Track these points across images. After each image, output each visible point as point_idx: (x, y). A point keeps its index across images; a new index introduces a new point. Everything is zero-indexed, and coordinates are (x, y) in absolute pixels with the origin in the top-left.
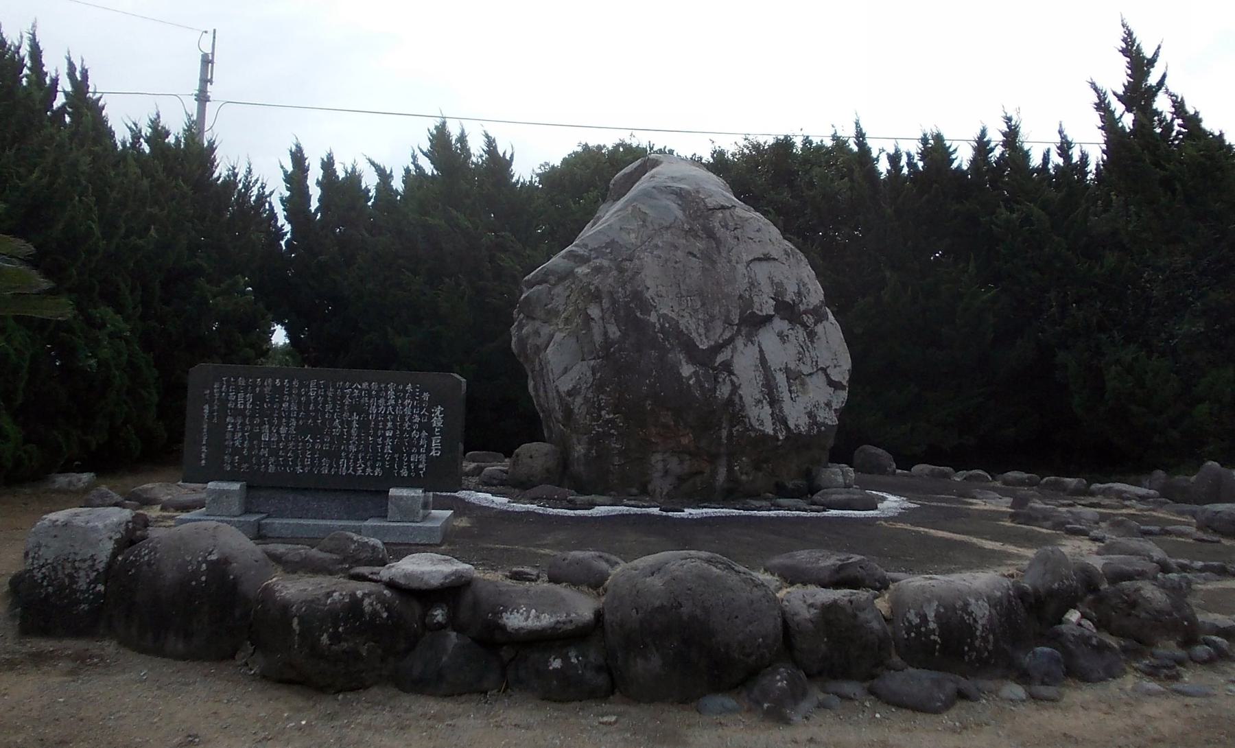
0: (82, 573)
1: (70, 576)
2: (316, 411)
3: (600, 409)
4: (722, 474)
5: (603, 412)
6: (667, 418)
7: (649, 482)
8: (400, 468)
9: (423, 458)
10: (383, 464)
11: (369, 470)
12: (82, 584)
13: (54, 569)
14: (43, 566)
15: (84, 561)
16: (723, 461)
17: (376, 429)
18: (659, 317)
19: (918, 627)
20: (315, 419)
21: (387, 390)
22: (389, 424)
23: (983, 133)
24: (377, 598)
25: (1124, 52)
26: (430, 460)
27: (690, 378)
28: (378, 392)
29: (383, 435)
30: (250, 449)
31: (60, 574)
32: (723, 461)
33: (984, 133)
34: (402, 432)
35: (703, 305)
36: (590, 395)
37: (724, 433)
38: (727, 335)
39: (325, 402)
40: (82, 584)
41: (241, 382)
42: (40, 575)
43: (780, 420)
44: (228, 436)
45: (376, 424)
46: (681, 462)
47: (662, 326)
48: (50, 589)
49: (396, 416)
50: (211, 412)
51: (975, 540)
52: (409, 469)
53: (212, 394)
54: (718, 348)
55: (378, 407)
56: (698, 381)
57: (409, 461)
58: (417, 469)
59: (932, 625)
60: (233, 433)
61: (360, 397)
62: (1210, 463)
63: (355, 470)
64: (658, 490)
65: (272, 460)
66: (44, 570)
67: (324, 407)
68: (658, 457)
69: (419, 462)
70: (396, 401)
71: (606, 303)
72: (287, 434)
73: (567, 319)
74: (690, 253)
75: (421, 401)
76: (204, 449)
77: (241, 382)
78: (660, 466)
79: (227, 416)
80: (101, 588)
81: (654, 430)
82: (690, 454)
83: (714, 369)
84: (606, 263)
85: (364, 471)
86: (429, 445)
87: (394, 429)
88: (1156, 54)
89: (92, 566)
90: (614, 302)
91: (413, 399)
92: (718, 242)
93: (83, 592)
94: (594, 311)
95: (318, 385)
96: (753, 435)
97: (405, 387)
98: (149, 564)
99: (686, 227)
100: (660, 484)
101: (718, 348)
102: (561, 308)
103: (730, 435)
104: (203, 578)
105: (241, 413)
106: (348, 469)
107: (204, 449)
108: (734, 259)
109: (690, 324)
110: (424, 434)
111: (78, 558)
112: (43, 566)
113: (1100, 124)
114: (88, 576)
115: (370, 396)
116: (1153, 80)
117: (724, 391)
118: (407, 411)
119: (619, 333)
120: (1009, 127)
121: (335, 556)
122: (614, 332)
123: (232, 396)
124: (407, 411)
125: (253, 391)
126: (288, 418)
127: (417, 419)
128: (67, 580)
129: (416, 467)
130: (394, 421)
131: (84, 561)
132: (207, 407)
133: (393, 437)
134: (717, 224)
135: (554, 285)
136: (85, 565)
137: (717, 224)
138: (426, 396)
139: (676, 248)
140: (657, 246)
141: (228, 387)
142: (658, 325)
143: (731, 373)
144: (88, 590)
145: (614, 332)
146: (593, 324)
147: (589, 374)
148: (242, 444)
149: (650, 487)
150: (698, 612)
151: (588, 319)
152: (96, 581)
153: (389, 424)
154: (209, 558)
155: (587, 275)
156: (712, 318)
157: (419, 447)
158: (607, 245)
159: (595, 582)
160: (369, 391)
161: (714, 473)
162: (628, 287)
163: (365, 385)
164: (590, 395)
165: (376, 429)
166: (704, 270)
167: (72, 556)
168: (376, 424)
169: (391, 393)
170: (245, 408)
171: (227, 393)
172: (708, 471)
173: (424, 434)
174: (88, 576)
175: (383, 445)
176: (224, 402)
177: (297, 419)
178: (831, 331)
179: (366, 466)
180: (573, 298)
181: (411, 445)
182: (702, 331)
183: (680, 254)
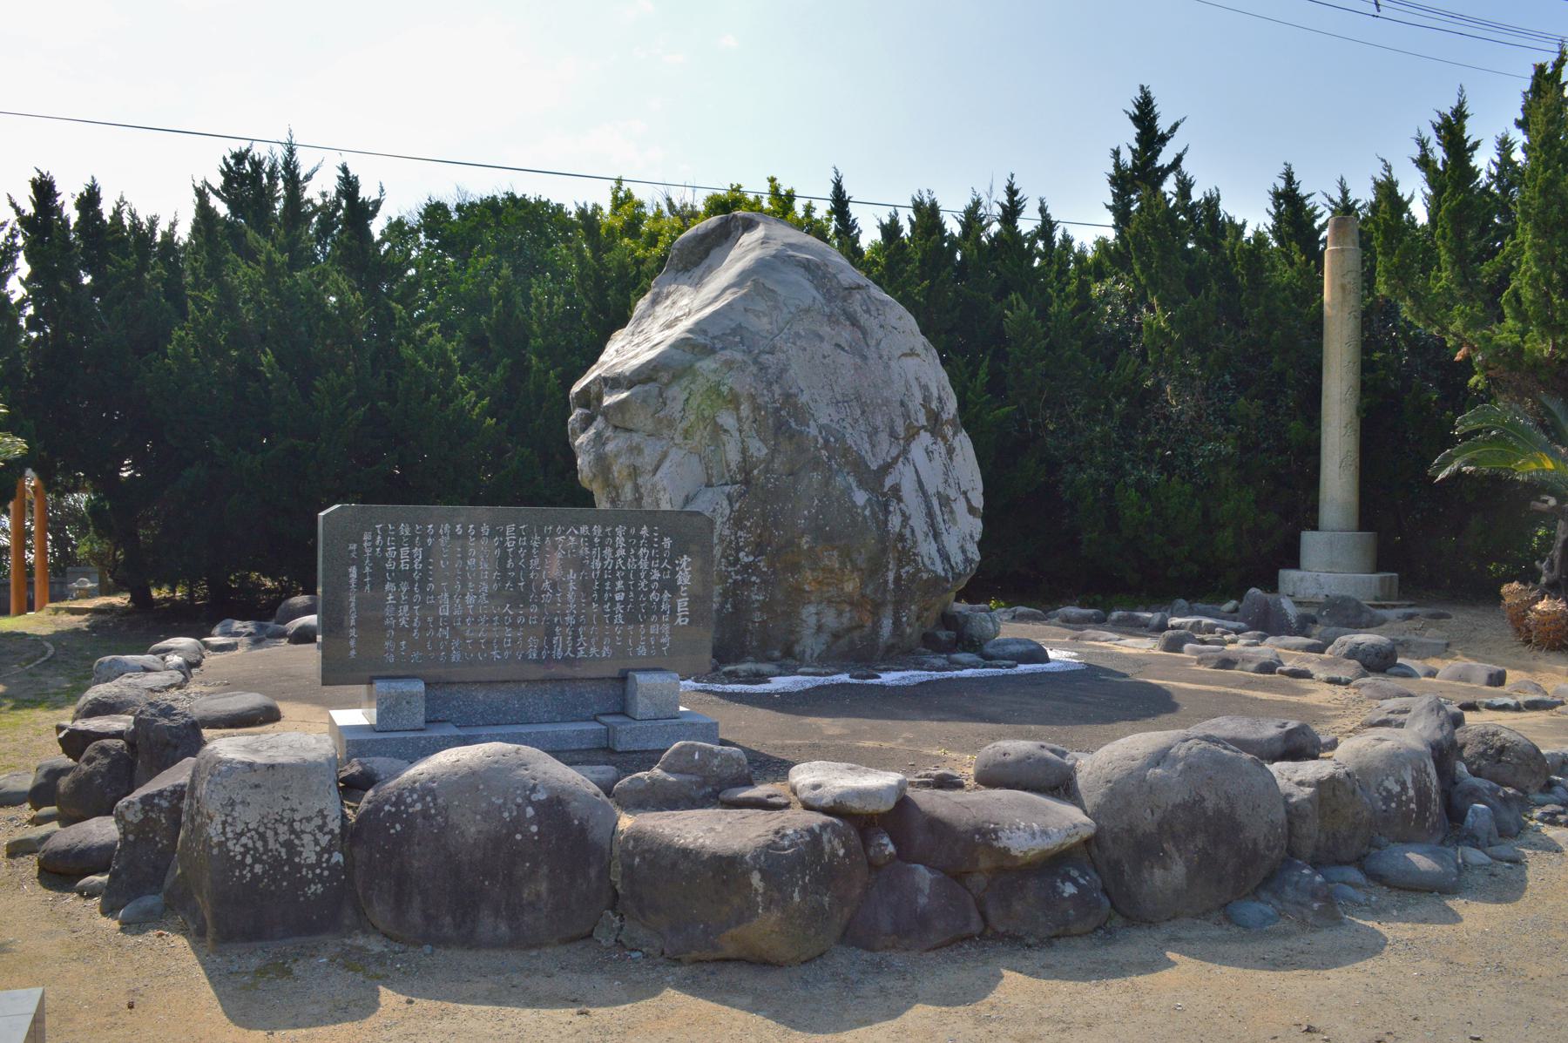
0: (307, 838)
1: (288, 845)
2: (517, 568)
3: (739, 549)
4: (887, 625)
5: (742, 554)
6: (832, 560)
7: (797, 641)
8: (636, 645)
9: (667, 627)
10: (613, 640)
11: (593, 650)
12: (309, 855)
13: (262, 837)
14: (242, 834)
15: (309, 819)
16: (888, 611)
17: (601, 591)
18: (821, 428)
19: (1399, 795)
20: (515, 581)
21: (614, 536)
22: (619, 584)
23: (977, 204)
24: (833, 831)
25: (1135, 119)
26: (675, 630)
27: (864, 508)
28: (604, 536)
29: (612, 599)
30: (424, 628)
31: (272, 845)
32: (888, 611)
33: (978, 203)
34: (637, 595)
35: (863, 412)
36: (726, 532)
37: (891, 576)
38: (894, 452)
39: (529, 556)
40: (309, 855)
41: (405, 530)
42: (239, 849)
43: (945, 557)
44: (388, 611)
45: (601, 585)
46: (840, 614)
47: (827, 441)
48: (258, 868)
49: (628, 571)
50: (361, 576)
51: (821, 680)
52: (648, 646)
53: (360, 550)
54: (886, 468)
55: (603, 559)
56: (873, 513)
57: (647, 634)
58: (659, 646)
59: (1411, 793)
60: (396, 607)
61: (577, 547)
62: (1253, 590)
63: (575, 651)
64: (808, 652)
65: (456, 643)
66: (244, 840)
67: (527, 563)
68: (812, 609)
69: (661, 635)
70: (628, 551)
71: (745, 409)
72: (476, 605)
73: (686, 431)
74: (838, 345)
75: (661, 549)
76: (353, 632)
77: (405, 530)
78: (812, 621)
79: (385, 582)
80: (337, 857)
81: (809, 575)
82: (851, 603)
83: (884, 495)
84: (739, 356)
85: (587, 651)
86: (674, 611)
87: (627, 590)
88: (1174, 128)
89: (321, 828)
90: (756, 408)
91: (650, 548)
92: (864, 333)
93: (311, 867)
94: (727, 419)
95: (518, 533)
96: (925, 576)
97: (638, 530)
98: (425, 814)
99: (827, 310)
100: (811, 644)
101: (886, 468)
102: (678, 415)
103: (898, 579)
104: (534, 829)
105: (406, 576)
106: (564, 651)
107: (353, 632)
108: (885, 353)
109: (856, 438)
110: (666, 595)
111: (297, 817)
112: (242, 834)
113: (1111, 203)
114: (317, 843)
115: (592, 545)
116: (1165, 159)
117: (895, 522)
118: (644, 564)
119: (765, 451)
120: (1011, 200)
121: (694, 778)
122: (758, 449)
123: (391, 552)
124: (644, 564)
125: (423, 544)
126: (477, 581)
127: (656, 575)
128: (283, 851)
129: (657, 641)
130: (625, 578)
131: (309, 819)
132: (353, 571)
133: (625, 602)
134: (859, 309)
135: (667, 385)
136: (309, 827)
137: (859, 309)
138: (667, 542)
139: (821, 339)
140: (798, 334)
141: (384, 538)
142: (821, 441)
143: (900, 500)
144: (319, 863)
145: (758, 449)
146: (725, 438)
147: (725, 503)
148: (410, 622)
149: (797, 649)
150: (1223, 804)
151: (718, 430)
152: (328, 849)
153: (619, 584)
154: (534, 797)
155: (715, 371)
156: (876, 431)
157: (660, 613)
158: (734, 332)
159: (1061, 785)
160: (590, 539)
161: (876, 626)
162: (776, 387)
163: (584, 529)
164: (726, 532)
165: (601, 591)
166: (857, 368)
167: (287, 814)
168: (601, 585)
169: (620, 540)
170: (412, 570)
171: (383, 550)
172: (869, 624)
173: (666, 595)
174: (317, 843)
175: (613, 613)
176: (378, 562)
177: (490, 582)
178: (964, 444)
179: (590, 645)
180: (694, 403)
181: (649, 612)
182: (867, 446)
183: (827, 347)
